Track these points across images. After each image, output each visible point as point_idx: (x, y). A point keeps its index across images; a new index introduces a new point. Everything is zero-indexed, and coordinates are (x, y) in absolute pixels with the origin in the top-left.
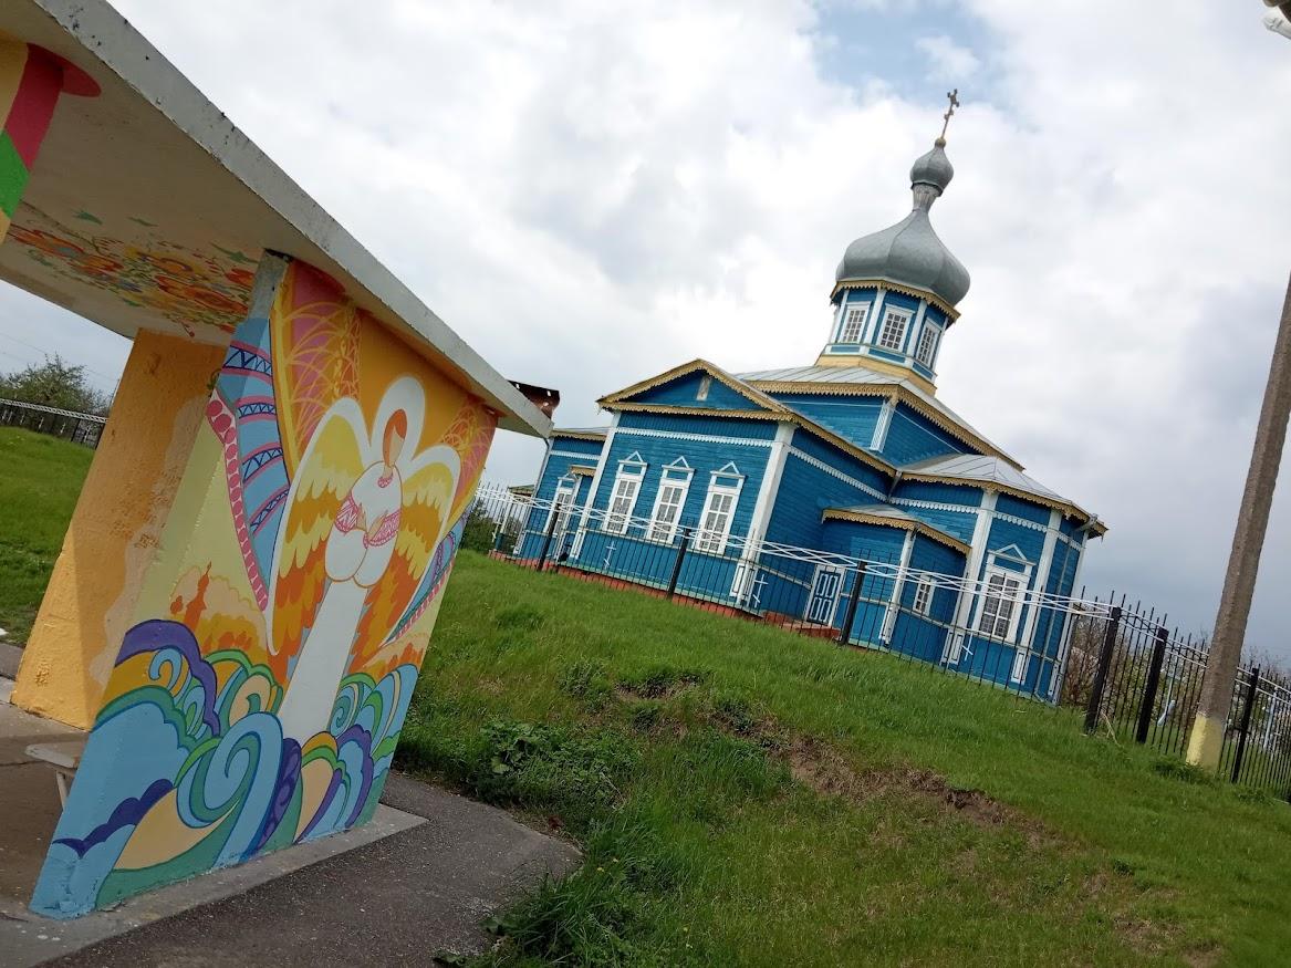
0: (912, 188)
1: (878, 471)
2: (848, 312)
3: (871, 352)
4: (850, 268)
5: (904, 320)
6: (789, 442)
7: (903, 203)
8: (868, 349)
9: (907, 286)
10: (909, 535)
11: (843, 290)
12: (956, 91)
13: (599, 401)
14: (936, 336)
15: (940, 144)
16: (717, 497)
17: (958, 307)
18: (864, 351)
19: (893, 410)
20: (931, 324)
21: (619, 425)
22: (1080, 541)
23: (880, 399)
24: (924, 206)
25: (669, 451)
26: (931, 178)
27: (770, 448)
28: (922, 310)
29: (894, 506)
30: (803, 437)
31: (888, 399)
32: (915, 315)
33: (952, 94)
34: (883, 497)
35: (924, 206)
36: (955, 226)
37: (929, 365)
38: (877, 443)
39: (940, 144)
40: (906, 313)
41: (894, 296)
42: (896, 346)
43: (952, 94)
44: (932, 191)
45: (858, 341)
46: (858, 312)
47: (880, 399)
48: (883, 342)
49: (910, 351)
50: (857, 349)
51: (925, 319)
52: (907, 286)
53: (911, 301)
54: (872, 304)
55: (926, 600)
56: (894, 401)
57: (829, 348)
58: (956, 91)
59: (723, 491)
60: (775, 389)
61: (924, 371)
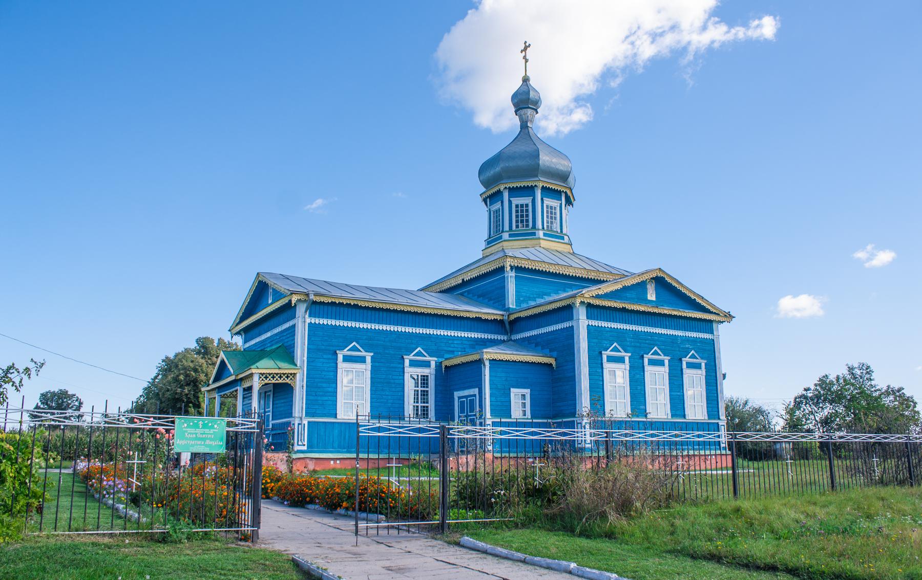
0: (516, 112)
3: (510, 236)
7: (511, 121)
14: (558, 209)
15: (526, 80)
22: (711, 332)
23: (501, 269)
25: (347, 336)
39: (526, 80)
40: (527, 200)
41: (514, 191)
42: (527, 226)
46: (522, 206)
48: (517, 226)
49: (539, 224)
51: (542, 199)
53: (529, 191)
54: (502, 202)
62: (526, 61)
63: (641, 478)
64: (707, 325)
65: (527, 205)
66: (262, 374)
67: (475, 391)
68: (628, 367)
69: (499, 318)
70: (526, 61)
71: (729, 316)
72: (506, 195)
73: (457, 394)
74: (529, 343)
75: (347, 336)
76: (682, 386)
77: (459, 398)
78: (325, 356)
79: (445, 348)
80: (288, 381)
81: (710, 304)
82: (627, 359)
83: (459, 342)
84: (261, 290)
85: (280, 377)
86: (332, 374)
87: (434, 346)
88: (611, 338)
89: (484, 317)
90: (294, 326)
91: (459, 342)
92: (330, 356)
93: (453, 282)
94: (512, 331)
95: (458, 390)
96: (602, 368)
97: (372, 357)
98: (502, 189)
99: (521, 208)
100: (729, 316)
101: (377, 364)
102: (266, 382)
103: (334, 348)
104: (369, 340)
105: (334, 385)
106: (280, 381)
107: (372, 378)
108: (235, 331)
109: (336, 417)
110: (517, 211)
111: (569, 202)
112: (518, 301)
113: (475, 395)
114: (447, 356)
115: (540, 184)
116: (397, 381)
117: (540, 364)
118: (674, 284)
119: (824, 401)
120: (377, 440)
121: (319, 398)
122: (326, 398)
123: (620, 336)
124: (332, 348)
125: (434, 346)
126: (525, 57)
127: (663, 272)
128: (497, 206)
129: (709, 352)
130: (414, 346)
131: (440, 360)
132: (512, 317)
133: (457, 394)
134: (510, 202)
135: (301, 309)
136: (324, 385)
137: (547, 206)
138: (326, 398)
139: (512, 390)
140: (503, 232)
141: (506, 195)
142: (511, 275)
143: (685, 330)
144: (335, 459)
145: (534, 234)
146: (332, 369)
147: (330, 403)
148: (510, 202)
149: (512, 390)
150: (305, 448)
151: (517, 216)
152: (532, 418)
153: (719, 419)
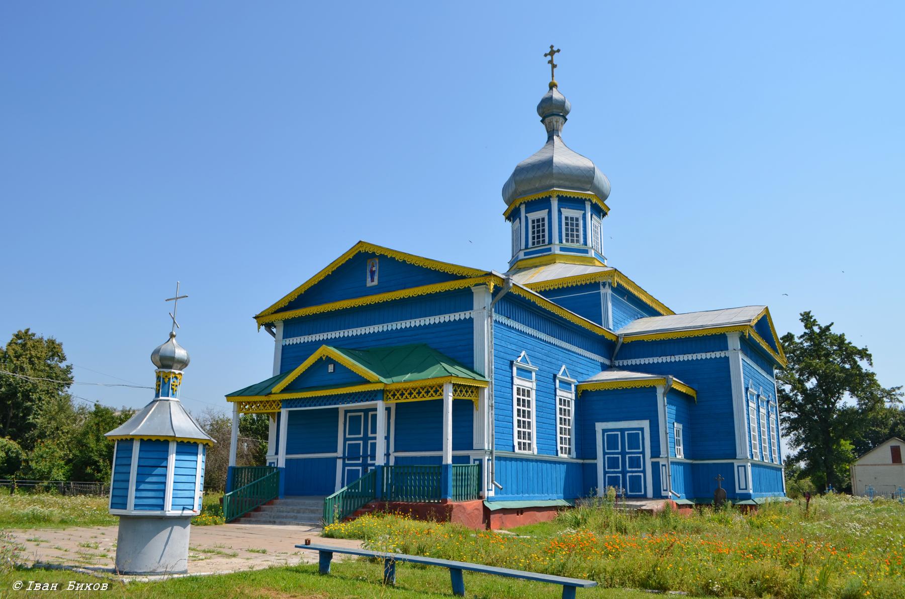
0: (542, 121)
3: (526, 254)
10: (173, 447)
12: (558, 51)
13: (255, 318)
40: (543, 214)
41: (564, 201)
51: (560, 211)
58: (558, 51)
63: (880, 514)
65: (543, 219)
66: (459, 385)
67: (645, 424)
70: (554, 66)
72: (555, 204)
73: (600, 426)
77: (604, 431)
99: (539, 222)
110: (567, 224)
111: (600, 212)
113: (642, 429)
120: (757, 469)
126: (551, 62)
127: (620, 274)
133: (600, 426)
134: (526, 217)
137: (567, 218)
139: (597, 424)
141: (555, 204)
145: (550, 250)
149: (597, 424)
151: (567, 230)
152: (577, 458)
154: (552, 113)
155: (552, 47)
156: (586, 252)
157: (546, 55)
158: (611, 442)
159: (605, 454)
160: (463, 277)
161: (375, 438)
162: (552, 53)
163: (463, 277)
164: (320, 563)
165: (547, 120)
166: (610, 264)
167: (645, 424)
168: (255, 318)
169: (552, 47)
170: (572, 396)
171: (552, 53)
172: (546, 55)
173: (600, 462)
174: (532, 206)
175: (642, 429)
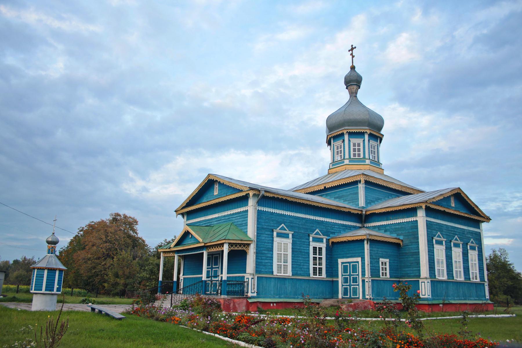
0: (347, 88)
1: (353, 213)
2: (335, 147)
3: (350, 162)
4: (331, 128)
5: (359, 145)
6: (425, 215)
7: (344, 96)
8: (348, 160)
9: (354, 128)
10: (365, 242)
11: (330, 138)
12: (355, 48)
13: (176, 211)
15: (353, 68)
16: (315, 248)
17: (382, 132)
18: (347, 162)
19: (364, 186)
20: (372, 142)
21: (187, 220)
22: (479, 228)
23: (356, 183)
24: (353, 95)
26: (353, 82)
27: (417, 221)
28: (366, 137)
29: (368, 228)
30: (429, 211)
31: (360, 181)
32: (364, 140)
33: (354, 47)
34: (359, 225)
35: (353, 95)
36: (370, 99)
37: (376, 160)
38: (362, 202)
39: (353, 68)
40: (359, 141)
41: (351, 134)
43: (354, 47)
44: (355, 87)
45: (362, 156)
47: (356, 183)
48: (354, 155)
49: (367, 156)
50: (343, 162)
51: (369, 141)
52: (354, 128)
53: (361, 134)
54: (344, 141)
55: (320, 264)
56: (363, 182)
57: (331, 165)
58: (355, 48)
59: (318, 245)
60: (310, 190)
61: (376, 163)
62: (353, 57)
64: (477, 224)
67: (359, 259)
68: (444, 247)
69: (360, 213)
70: (353, 57)
71: (488, 219)
72: (346, 137)
74: (379, 230)
75: (280, 220)
76: (468, 260)
77: (342, 263)
78: (266, 233)
79: (331, 231)
80: (244, 248)
81: (481, 211)
82: (290, 236)
83: (337, 227)
84: (209, 184)
85: (240, 246)
86: (270, 244)
87: (327, 230)
88: (437, 229)
89: (352, 211)
90: (247, 211)
91: (337, 227)
92: (269, 233)
93: (316, 189)
94: (366, 222)
95: (343, 257)
96: (433, 248)
97: (293, 234)
98: (345, 132)
100: (488, 219)
101: (295, 239)
102: (232, 249)
103: (272, 228)
104: (291, 223)
105: (271, 252)
106: (240, 249)
107: (292, 248)
108: (179, 212)
109: (273, 274)
112: (368, 202)
113: (358, 262)
114: (331, 235)
115: (368, 132)
116: (305, 251)
117: (394, 243)
118: (465, 198)
119: (121, 250)
121: (263, 261)
122: (267, 261)
123: (440, 227)
124: (270, 228)
125: (327, 230)
128: (339, 143)
129: (478, 238)
130: (314, 228)
131: (328, 238)
132: (368, 213)
133: (340, 261)
135: (252, 202)
136: (266, 252)
137: (354, 145)
138: (267, 261)
140: (344, 159)
141: (346, 137)
142: (361, 187)
143: (468, 226)
144: (273, 303)
146: (270, 242)
147: (269, 264)
148: (349, 140)
150: (255, 294)
153: (485, 281)
154: (353, 82)
155: (352, 46)
156: (365, 161)
157: (349, 51)
158: (345, 269)
159: (342, 275)
160: (479, 215)
161: (208, 268)
162: (352, 49)
163: (479, 215)
164: (31, 311)
165: (349, 88)
166: (139, 235)
167: (359, 259)
168: (176, 211)
169: (352, 46)
170: (323, 246)
171: (352, 49)
172: (349, 51)
173: (340, 279)
174: (336, 137)
175: (358, 262)
